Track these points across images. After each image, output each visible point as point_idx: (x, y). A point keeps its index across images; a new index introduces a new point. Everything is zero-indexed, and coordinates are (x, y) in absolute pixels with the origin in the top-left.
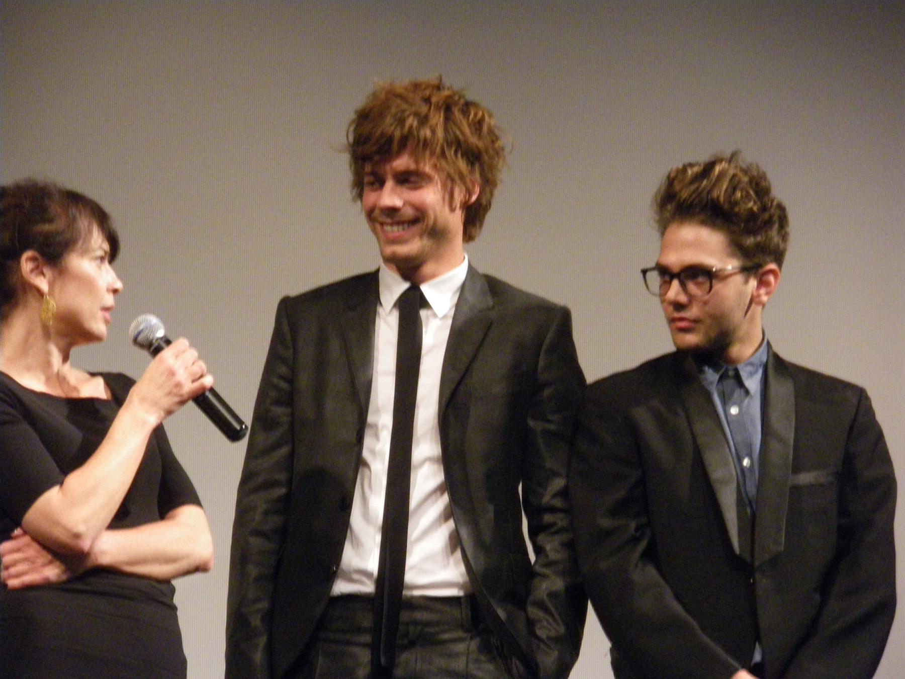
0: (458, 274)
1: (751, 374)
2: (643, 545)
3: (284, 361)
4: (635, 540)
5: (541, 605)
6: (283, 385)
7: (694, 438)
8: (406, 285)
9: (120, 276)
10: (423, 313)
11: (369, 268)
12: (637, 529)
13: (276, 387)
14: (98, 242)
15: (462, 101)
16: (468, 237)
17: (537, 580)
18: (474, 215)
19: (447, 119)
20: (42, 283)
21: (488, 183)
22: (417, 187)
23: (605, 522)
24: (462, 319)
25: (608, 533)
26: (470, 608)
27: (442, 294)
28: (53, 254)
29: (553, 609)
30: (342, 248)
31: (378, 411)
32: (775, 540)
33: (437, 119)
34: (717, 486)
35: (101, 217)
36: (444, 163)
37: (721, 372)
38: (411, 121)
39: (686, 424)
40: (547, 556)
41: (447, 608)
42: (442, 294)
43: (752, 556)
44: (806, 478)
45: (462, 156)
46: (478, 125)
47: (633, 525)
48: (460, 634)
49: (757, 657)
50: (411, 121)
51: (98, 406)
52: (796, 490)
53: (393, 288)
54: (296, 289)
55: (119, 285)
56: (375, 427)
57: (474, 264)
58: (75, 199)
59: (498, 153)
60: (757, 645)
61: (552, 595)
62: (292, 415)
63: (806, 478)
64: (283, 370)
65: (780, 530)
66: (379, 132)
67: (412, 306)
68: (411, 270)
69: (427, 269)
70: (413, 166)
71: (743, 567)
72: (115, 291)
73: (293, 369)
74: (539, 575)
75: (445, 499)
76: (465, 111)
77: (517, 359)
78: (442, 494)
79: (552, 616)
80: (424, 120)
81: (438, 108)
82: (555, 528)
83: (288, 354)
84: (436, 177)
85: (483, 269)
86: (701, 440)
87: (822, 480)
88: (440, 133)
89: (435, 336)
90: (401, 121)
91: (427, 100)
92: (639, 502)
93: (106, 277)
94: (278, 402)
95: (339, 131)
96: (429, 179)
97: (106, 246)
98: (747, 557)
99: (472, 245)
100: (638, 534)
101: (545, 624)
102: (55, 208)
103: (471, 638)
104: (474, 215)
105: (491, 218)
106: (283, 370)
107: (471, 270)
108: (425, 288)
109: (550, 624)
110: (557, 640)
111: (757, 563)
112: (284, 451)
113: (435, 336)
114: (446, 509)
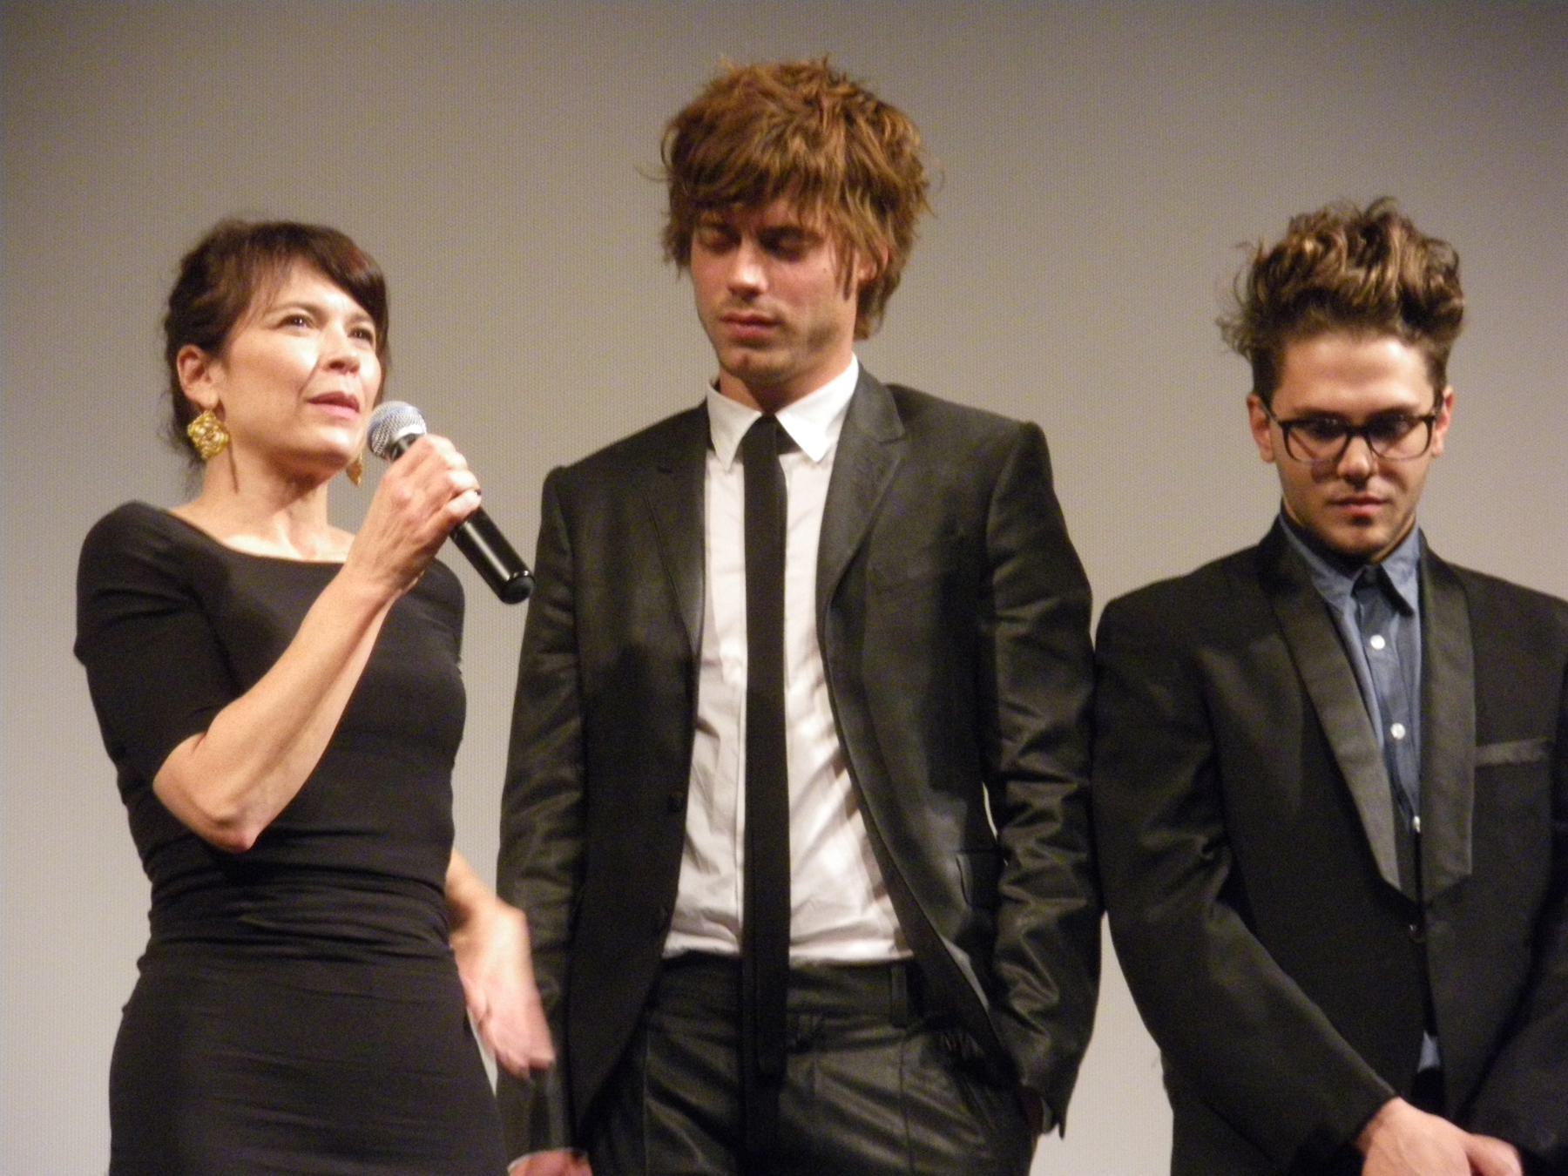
1: (1405, 577)
2: (1222, 873)
3: (558, 576)
4: (1208, 867)
5: (1020, 958)
6: (562, 617)
7: (1303, 684)
8: (757, 414)
10: (787, 461)
12: (1206, 849)
13: (550, 623)
15: (871, 105)
16: (861, 333)
17: (1008, 908)
18: (872, 297)
19: (851, 137)
21: (903, 242)
22: (794, 256)
23: (1154, 839)
24: (748, 397)
25: (1156, 858)
26: (913, 990)
27: (815, 422)
29: (1040, 965)
32: (1455, 857)
33: (836, 140)
34: (1347, 768)
36: (843, 216)
37: (1357, 576)
38: (797, 144)
39: (1288, 665)
40: (1018, 865)
41: (862, 985)
42: (815, 422)
43: (1419, 887)
44: (1500, 753)
45: (873, 202)
46: (895, 150)
47: (1201, 840)
48: (887, 1031)
49: (1429, 1056)
50: (797, 144)
52: (1485, 773)
53: (734, 421)
54: (572, 452)
56: (716, 664)
57: (867, 368)
59: (918, 192)
60: (1426, 1036)
61: (1034, 935)
62: (578, 665)
63: (1500, 753)
64: (561, 592)
65: (1463, 837)
66: (741, 161)
67: (765, 450)
68: (772, 392)
70: (793, 219)
71: (1404, 909)
73: (574, 586)
74: (1009, 899)
75: (844, 781)
76: (877, 125)
77: (962, 540)
78: (838, 773)
79: (1031, 968)
80: (814, 141)
81: (834, 118)
82: (1029, 813)
83: (565, 563)
84: (830, 238)
85: (884, 377)
86: (1314, 690)
87: (1526, 756)
88: (840, 162)
89: (806, 492)
90: (780, 142)
91: (812, 102)
92: (1211, 797)
94: (551, 649)
95: (647, 152)
96: (817, 240)
98: (1411, 894)
99: (864, 344)
100: (1209, 857)
101: (1022, 986)
103: (909, 1037)
104: (872, 297)
105: (896, 301)
106: (561, 592)
107: (865, 379)
108: (788, 419)
109: (1034, 988)
110: (1048, 1014)
111: (1427, 897)
112: (574, 725)
113: (806, 492)
114: (848, 798)
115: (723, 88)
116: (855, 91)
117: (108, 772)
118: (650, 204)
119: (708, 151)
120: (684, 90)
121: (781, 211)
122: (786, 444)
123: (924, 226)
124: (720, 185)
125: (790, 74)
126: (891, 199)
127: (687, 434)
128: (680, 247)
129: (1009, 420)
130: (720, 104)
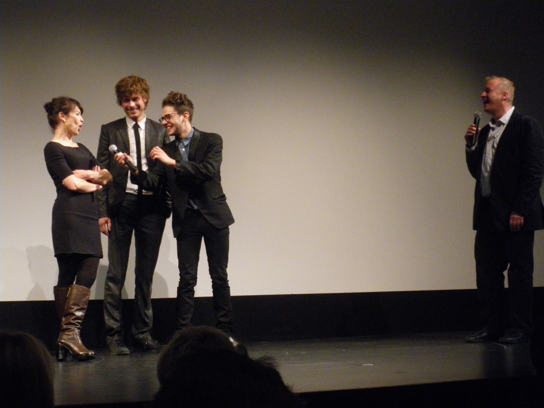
0: (144, 120)
8: (135, 123)
9: (83, 118)
11: (122, 117)
14: (77, 109)
20: (64, 119)
27: (142, 124)
28: (66, 112)
30: (119, 113)
31: (132, 152)
33: (139, 85)
35: (78, 104)
38: (134, 86)
42: (142, 124)
46: (146, 84)
50: (134, 86)
51: (162, 146)
54: (105, 123)
55: (83, 120)
58: (72, 101)
67: (136, 128)
68: (135, 119)
69: (139, 119)
72: (81, 121)
93: (79, 118)
97: (79, 111)
102: (67, 102)
107: (147, 119)
108: (139, 124)
112: (108, 161)
115: (123, 81)
116: (138, 78)
117: (51, 182)
118: (115, 98)
119: (123, 89)
120: (116, 82)
121: (134, 96)
122: (139, 127)
123: (150, 93)
124: (124, 93)
125: (130, 77)
126: (146, 91)
127: (121, 124)
128: (120, 103)
129: (219, 161)
130: (122, 83)
